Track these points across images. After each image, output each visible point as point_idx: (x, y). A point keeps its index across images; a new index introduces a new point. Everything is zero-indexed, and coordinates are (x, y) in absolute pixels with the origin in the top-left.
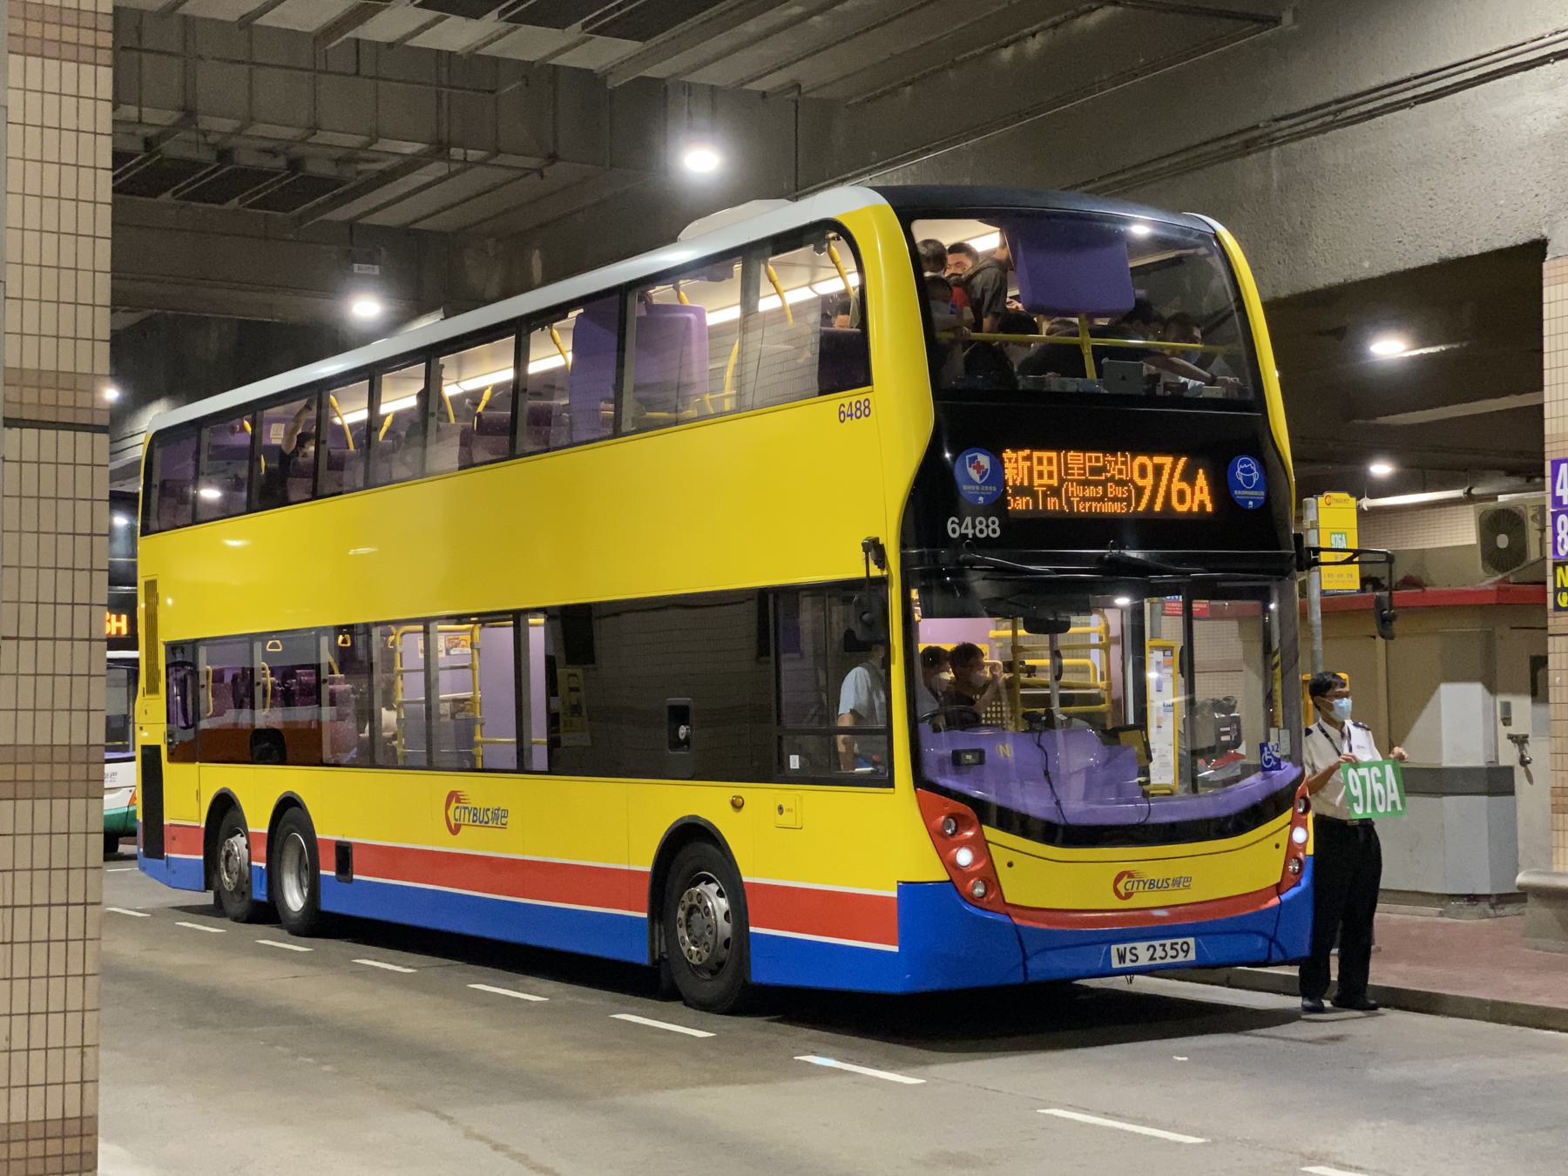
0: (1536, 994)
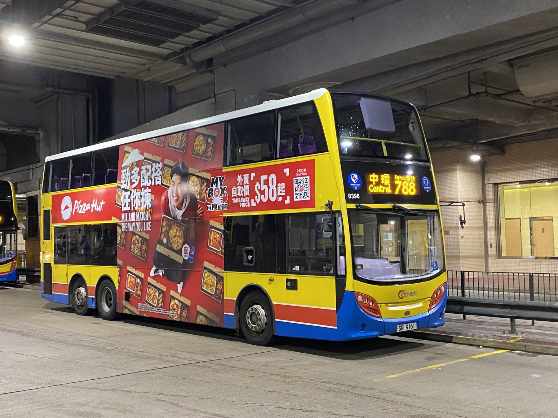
0: (147, 333)
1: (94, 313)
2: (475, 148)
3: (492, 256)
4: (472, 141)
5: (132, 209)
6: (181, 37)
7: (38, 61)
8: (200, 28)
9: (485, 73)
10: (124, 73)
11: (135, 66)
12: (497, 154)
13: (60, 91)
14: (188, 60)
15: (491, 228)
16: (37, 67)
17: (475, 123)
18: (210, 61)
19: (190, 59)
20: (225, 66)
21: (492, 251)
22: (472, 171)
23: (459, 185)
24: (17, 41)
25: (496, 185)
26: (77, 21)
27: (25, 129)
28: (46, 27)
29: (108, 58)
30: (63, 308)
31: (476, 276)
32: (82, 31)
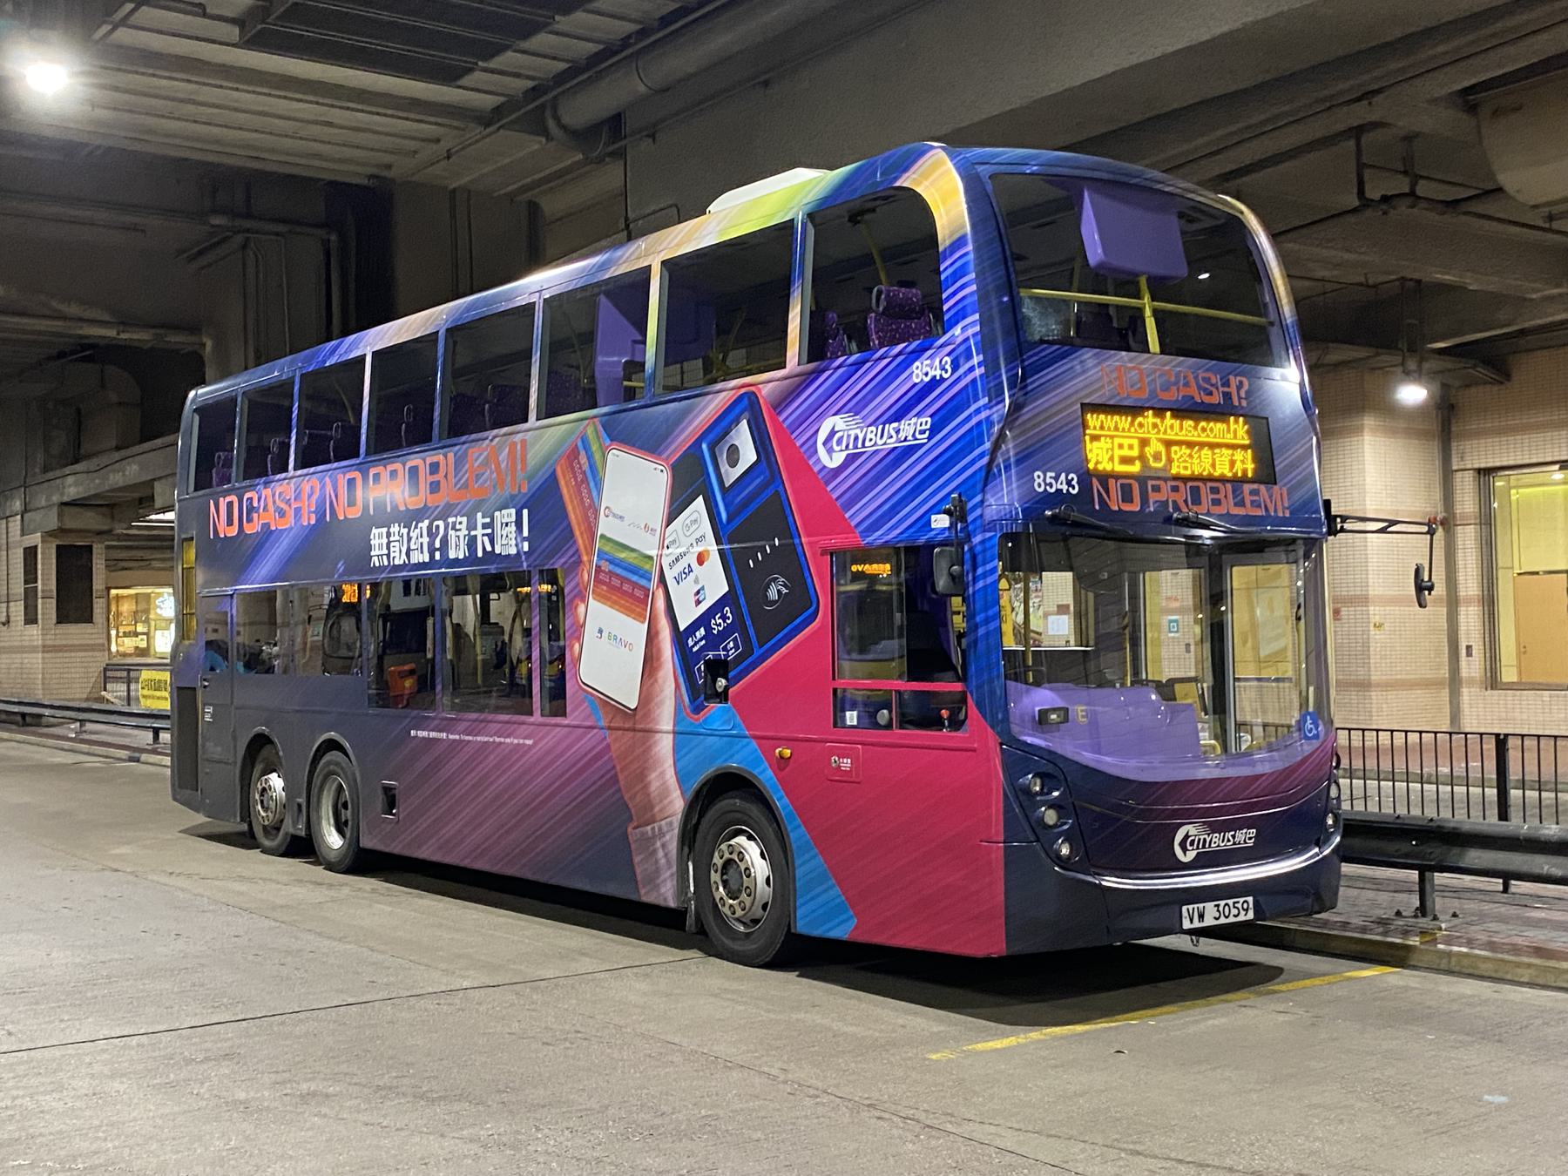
1: (303, 847)
2: (1412, 365)
3: (1471, 681)
4: (1403, 345)
5: (1169, 594)
6: (510, 54)
7: (137, 135)
8: (557, 27)
9: (1409, 139)
10: (389, 167)
11: (413, 145)
12: (1485, 383)
13: (248, 224)
14: (551, 123)
15: (1469, 601)
16: (110, 149)
17: (1416, 290)
18: (615, 124)
19: (557, 119)
20: (653, 136)
21: (1472, 667)
22: (1410, 433)
23: (1375, 473)
24: (51, 80)
25: (1485, 473)
26: (204, 15)
27: (161, 331)
28: (124, 35)
29: (330, 124)
30: (231, 834)
31: (1357, 743)
32: (233, 45)
